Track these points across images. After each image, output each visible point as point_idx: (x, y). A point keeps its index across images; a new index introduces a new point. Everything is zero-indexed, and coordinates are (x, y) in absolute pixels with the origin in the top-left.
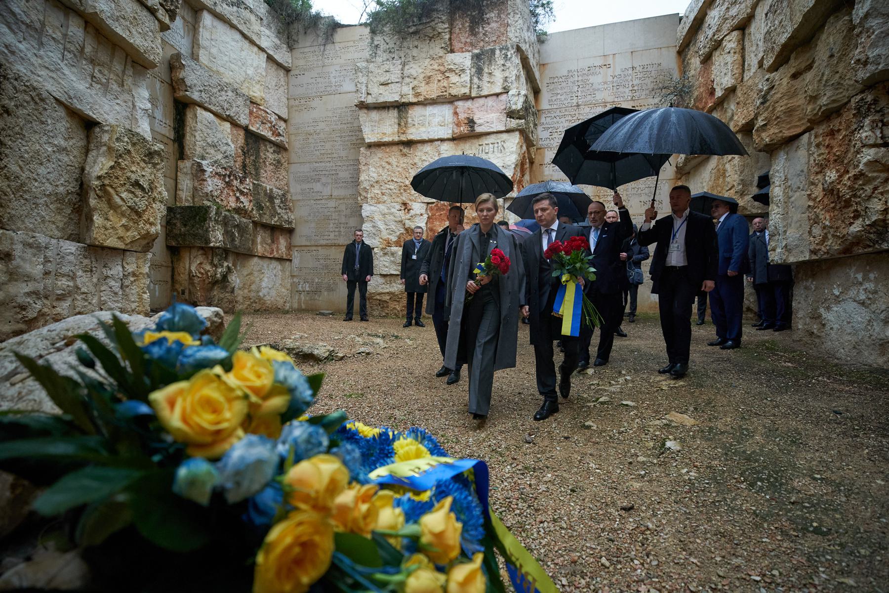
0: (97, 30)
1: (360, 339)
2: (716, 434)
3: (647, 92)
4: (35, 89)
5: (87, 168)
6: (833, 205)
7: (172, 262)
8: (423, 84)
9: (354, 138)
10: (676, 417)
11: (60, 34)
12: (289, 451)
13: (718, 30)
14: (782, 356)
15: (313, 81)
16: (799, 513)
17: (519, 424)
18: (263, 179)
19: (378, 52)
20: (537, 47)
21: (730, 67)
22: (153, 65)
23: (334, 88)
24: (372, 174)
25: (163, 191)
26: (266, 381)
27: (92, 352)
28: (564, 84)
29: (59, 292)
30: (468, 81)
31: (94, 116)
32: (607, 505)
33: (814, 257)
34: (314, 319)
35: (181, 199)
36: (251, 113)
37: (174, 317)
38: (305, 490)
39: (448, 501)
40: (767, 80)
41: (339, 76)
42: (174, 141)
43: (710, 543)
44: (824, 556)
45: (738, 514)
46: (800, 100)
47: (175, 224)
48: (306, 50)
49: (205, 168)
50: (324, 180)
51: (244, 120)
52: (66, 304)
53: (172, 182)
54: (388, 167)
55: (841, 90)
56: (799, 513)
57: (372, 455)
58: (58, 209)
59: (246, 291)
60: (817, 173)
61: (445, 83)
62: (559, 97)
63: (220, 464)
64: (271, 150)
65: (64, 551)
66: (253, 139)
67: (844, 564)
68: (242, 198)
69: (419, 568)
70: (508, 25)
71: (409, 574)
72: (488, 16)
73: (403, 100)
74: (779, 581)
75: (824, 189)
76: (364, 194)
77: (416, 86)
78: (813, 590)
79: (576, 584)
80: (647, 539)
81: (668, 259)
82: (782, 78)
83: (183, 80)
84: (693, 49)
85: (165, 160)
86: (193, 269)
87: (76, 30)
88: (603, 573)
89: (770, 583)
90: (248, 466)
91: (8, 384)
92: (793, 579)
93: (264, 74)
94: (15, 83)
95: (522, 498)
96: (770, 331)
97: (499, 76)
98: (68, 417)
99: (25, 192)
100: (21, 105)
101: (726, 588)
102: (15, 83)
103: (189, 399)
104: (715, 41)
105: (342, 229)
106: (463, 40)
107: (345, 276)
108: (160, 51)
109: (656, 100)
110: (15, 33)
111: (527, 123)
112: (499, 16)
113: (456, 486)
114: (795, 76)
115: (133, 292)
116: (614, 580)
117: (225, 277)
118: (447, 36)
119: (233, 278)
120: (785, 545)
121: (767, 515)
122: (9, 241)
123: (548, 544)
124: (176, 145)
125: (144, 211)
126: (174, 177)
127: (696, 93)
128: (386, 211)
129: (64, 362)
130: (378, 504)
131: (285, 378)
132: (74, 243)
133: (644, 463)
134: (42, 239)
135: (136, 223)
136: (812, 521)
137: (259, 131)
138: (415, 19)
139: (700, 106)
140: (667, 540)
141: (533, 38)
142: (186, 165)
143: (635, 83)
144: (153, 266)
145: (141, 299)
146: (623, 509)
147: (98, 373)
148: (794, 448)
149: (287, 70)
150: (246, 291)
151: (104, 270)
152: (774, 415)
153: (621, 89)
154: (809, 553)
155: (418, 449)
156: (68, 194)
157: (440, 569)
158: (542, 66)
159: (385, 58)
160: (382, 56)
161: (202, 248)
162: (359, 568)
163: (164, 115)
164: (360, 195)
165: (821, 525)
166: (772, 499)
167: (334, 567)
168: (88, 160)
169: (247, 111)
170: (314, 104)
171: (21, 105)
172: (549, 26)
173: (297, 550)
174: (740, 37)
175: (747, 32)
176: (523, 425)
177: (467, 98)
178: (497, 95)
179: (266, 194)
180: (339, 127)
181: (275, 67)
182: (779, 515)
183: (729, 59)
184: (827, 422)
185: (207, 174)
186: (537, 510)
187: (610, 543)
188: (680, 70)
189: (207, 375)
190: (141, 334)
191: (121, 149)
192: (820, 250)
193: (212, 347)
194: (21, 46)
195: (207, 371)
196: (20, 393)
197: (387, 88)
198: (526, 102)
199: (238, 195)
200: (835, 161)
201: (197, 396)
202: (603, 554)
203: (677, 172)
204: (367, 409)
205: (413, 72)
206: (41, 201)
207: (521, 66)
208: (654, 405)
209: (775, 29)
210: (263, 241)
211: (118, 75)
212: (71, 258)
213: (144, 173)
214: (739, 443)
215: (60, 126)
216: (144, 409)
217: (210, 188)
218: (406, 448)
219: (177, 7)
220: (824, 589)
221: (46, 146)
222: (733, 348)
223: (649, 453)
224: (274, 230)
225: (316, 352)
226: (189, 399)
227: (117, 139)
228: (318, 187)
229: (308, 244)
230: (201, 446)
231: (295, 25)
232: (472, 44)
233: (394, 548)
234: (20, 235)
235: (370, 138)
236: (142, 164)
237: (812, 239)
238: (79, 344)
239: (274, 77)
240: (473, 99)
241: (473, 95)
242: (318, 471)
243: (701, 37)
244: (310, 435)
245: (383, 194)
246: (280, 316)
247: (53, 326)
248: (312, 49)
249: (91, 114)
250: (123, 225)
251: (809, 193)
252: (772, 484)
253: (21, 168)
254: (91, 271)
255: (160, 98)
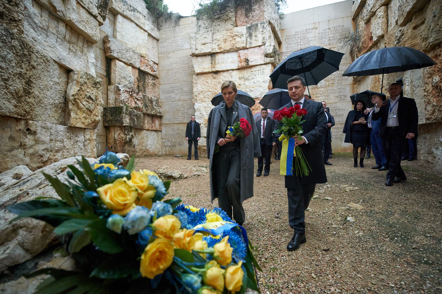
0: (71, 27)
1: (195, 168)
2: (374, 214)
3: (337, 40)
4: (45, 56)
5: (68, 91)
6: (438, 94)
7: (106, 133)
8: (223, 43)
9: (190, 71)
10: (353, 205)
11: (55, 31)
12: (155, 214)
13: (374, 7)
14: (412, 174)
15: (170, 44)
16: (417, 253)
17: (273, 209)
18: (147, 93)
19: (201, 29)
20: (279, 21)
21: (380, 25)
22: (96, 42)
23: (180, 47)
24: (199, 88)
25: (101, 101)
26: (145, 184)
27: (74, 172)
28: (293, 39)
29: (57, 149)
30: (245, 40)
31: (71, 67)
32: (316, 248)
33: (428, 122)
34: (173, 159)
35: (110, 103)
36: (141, 61)
37: (107, 157)
38: (162, 229)
39: (227, 237)
40: (400, 31)
41: (182, 42)
42: (106, 76)
43: (368, 268)
44: (429, 275)
45: (384, 254)
46: (418, 40)
47: (107, 116)
48: (166, 30)
49: (120, 88)
50: (176, 92)
51: (138, 65)
52: (59, 154)
53: (105, 96)
54: (207, 84)
55: (440, 34)
56: (417, 253)
57: (196, 220)
58: (55, 110)
59: (140, 146)
60: (429, 78)
61: (233, 42)
62: (291, 45)
63: (126, 218)
64: (151, 79)
65: (64, 256)
66: (142, 74)
67: (440, 280)
68: (138, 102)
69: (212, 266)
70: (264, 11)
71: (208, 269)
72: (254, 7)
73: (213, 51)
74: (405, 287)
75: (432, 86)
76: (196, 98)
77: (219, 44)
78: (423, 292)
79: (299, 286)
80: (336, 265)
81: (388, 123)
82: (408, 29)
83: (109, 48)
84: (360, 17)
85: (102, 86)
86: (116, 136)
87: (62, 28)
88: (312, 281)
89: (399, 288)
90: (137, 219)
91: (38, 189)
92: (412, 286)
93: (147, 42)
94: (37, 54)
95: (273, 245)
96: (406, 161)
97: (260, 37)
98: (64, 201)
99: (41, 103)
100: (39, 64)
101: (376, 289)
102: (37, 54)
103: (113, 191)
104: (372, 12)
105: (185, 115)
106: (242, 20)
107: (187, 138)
108: (99, 35)
109: (342, 44)
110: (36, 32)
111: (275, 59)
112: (259, 7)
113: (233, 233)
114: (415, 28)
115: (89, 148)
116: (318, 284)
117: (130, 140)
118: (234, 19)
119: (134, 140)
120: (408, 269)
121: (400, 254)
122: (35, 126)
123: (285, 267)
124: (107, 78)
125: (93, 110)
126: (106, 93)
127: (363, 40)
128: (206, 106)
129: (63, 178)
130: (195, 239)
131: (154, 183)
132: (63, 126)
133: (335, 228)
134: (49, 125)
135: (90, 116)
136: (424, 258)
137: (145, 70)
138: (218, 12)
139: (365, 46)
140: (346, 266)
141: (277, 17)
142: (112, 88)
143: (330, 36)
144: (98, 136)
145: (92, 151)
146: (324, 250)
147: (76, 182)
148: (416, 221)
149: (158, 40)
150: (140, 146)
151: (76, 138)
152: (406, 204)
153: (323, 40)
154: (421, 273)
155: (217, 217)
156: (60, 103)
157: (222, 268)
158: (282, 30)
159: (204, 32)
160: (202, 30)
161: (120, 126)
162: (185, 263)
163: (102, 65)
164: (194, 98)
165: (429, 260)
166: (402, 246)
167: (174, 263)
168: (68, 87)
169: (139, 61)
170: (170, 55)
171: (39, 64)
172: (284, 10)
173: (158, 254)
174: (386, 9)
175: (389, 6)
176: (274, 209)
177: (245, 48)
178: (260, 46)
179: (149, 100)
180: (183, 66)
181: (152, 39)
182: (406, 255)
183: (380, 21)
184: (435, 207)
185: (121, 91)
186: (280, 250)
187: (317, 267)
188: (354, 28)
189: (120, 181)
190: (93, 165)
191: (83, 82)
192: (431, 118)
193: (123, 170)
194: (39, 38)
195: (120, 179)
196: (43, 192)
197: (205, 46)
198: (274, 49)
199: (136, 100)
200: (438, 71)
201: (116, 190)
202: (313, 272)
203: (354, 81)
204: (198, 202)
205: (218, 37)
206: (48, 107)
207: (271, 31)
208: (341, 199)
209: (404, 4)
210: (148, 123)
211: (80, 48)
212: (62, 133)
213: (92, 92)
214: (386, 218)
215: (56, 72)
216: (95, 195)
217: (123, 98)
218: (212, 217)
219: (106, 14)
220: (428, 291)
221: (50, 82)
222: (385, 170)
223: (338, 223)
224: (154, 117)
225: (173, 175)
226: (113, 191)
227: (81, 77)
228: (173, 95)
229: (170, 123)
230: (118, 211)
231: (161, 18)
232: (246, 22)
233: (203, 258)
234: (40, 123)
235: (198, 70)
236: (92, 88)
237: (426, 112)
238: (69, 169)
239: (152, 43)
240: (247, 49)
241: (247, 47)
242: (167, 222)
243: (365, 11)
244: (164, 207)
245: (205, 98)
246: (157, 158)
247: (55, 164)
248: (169, 29)
249: (69, 66)
250: (84, 117)
251: (424, 88)
252: (403, 239)
253: (40, 92)
254: (70, 139)
255: (99, 57)
